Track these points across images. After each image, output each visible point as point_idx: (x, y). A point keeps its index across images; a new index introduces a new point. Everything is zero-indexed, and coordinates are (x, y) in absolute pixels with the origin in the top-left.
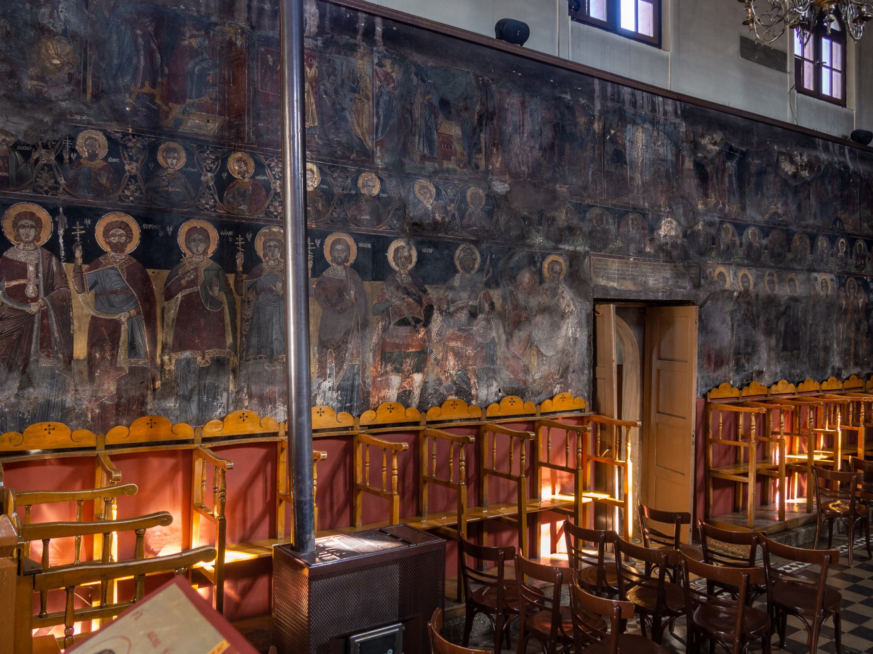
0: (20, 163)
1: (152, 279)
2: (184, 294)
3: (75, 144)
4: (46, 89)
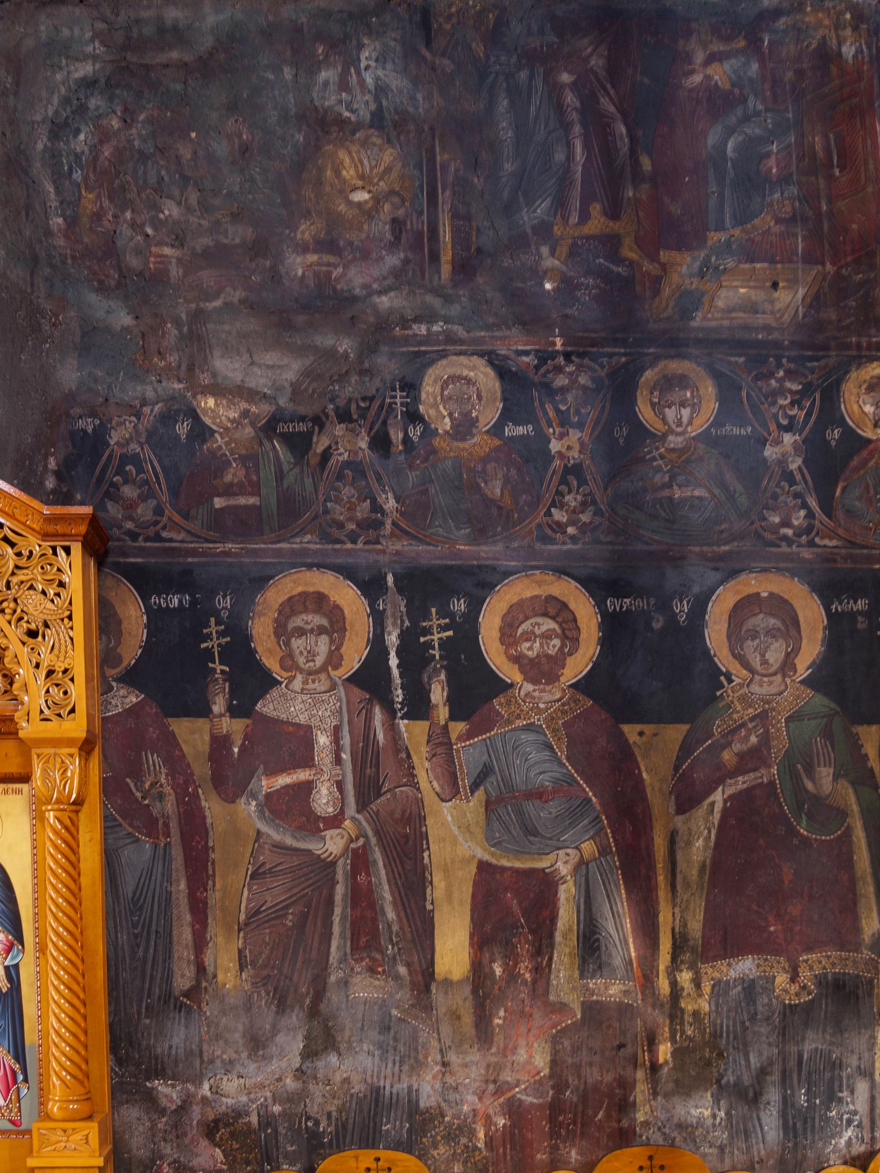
0: (286, 467)
1: (636, 751)
2: (730, 791)
3: (417, 400)
4: (340, 270)
